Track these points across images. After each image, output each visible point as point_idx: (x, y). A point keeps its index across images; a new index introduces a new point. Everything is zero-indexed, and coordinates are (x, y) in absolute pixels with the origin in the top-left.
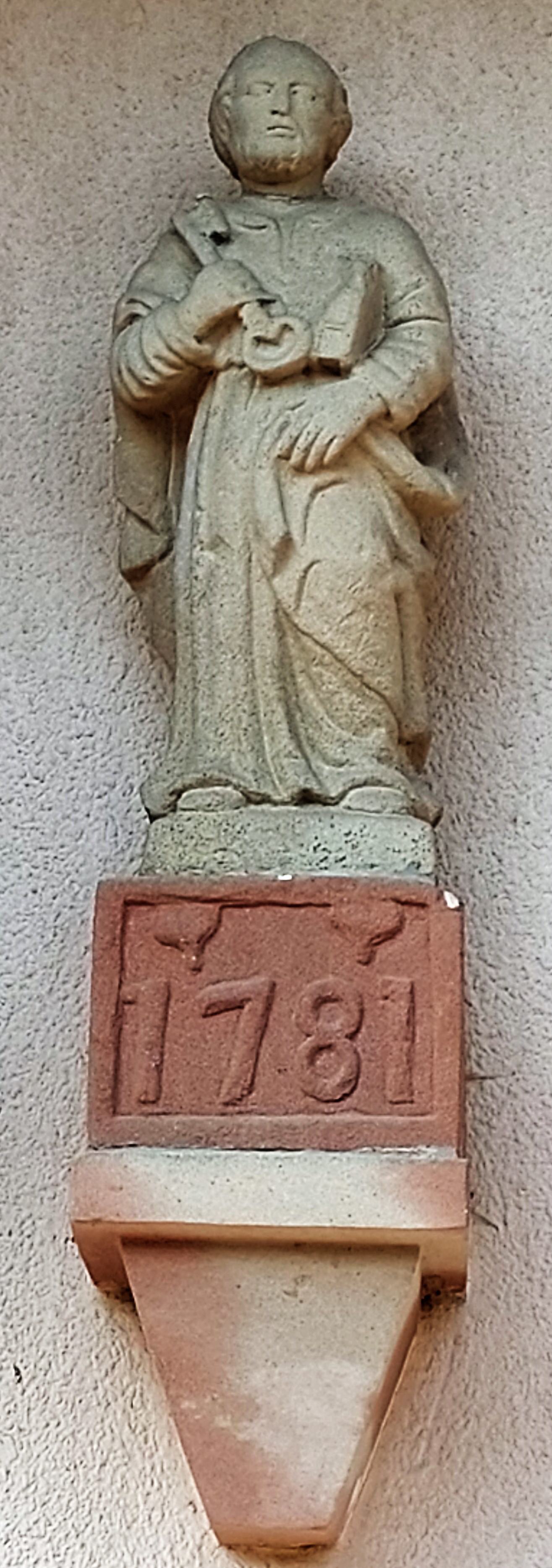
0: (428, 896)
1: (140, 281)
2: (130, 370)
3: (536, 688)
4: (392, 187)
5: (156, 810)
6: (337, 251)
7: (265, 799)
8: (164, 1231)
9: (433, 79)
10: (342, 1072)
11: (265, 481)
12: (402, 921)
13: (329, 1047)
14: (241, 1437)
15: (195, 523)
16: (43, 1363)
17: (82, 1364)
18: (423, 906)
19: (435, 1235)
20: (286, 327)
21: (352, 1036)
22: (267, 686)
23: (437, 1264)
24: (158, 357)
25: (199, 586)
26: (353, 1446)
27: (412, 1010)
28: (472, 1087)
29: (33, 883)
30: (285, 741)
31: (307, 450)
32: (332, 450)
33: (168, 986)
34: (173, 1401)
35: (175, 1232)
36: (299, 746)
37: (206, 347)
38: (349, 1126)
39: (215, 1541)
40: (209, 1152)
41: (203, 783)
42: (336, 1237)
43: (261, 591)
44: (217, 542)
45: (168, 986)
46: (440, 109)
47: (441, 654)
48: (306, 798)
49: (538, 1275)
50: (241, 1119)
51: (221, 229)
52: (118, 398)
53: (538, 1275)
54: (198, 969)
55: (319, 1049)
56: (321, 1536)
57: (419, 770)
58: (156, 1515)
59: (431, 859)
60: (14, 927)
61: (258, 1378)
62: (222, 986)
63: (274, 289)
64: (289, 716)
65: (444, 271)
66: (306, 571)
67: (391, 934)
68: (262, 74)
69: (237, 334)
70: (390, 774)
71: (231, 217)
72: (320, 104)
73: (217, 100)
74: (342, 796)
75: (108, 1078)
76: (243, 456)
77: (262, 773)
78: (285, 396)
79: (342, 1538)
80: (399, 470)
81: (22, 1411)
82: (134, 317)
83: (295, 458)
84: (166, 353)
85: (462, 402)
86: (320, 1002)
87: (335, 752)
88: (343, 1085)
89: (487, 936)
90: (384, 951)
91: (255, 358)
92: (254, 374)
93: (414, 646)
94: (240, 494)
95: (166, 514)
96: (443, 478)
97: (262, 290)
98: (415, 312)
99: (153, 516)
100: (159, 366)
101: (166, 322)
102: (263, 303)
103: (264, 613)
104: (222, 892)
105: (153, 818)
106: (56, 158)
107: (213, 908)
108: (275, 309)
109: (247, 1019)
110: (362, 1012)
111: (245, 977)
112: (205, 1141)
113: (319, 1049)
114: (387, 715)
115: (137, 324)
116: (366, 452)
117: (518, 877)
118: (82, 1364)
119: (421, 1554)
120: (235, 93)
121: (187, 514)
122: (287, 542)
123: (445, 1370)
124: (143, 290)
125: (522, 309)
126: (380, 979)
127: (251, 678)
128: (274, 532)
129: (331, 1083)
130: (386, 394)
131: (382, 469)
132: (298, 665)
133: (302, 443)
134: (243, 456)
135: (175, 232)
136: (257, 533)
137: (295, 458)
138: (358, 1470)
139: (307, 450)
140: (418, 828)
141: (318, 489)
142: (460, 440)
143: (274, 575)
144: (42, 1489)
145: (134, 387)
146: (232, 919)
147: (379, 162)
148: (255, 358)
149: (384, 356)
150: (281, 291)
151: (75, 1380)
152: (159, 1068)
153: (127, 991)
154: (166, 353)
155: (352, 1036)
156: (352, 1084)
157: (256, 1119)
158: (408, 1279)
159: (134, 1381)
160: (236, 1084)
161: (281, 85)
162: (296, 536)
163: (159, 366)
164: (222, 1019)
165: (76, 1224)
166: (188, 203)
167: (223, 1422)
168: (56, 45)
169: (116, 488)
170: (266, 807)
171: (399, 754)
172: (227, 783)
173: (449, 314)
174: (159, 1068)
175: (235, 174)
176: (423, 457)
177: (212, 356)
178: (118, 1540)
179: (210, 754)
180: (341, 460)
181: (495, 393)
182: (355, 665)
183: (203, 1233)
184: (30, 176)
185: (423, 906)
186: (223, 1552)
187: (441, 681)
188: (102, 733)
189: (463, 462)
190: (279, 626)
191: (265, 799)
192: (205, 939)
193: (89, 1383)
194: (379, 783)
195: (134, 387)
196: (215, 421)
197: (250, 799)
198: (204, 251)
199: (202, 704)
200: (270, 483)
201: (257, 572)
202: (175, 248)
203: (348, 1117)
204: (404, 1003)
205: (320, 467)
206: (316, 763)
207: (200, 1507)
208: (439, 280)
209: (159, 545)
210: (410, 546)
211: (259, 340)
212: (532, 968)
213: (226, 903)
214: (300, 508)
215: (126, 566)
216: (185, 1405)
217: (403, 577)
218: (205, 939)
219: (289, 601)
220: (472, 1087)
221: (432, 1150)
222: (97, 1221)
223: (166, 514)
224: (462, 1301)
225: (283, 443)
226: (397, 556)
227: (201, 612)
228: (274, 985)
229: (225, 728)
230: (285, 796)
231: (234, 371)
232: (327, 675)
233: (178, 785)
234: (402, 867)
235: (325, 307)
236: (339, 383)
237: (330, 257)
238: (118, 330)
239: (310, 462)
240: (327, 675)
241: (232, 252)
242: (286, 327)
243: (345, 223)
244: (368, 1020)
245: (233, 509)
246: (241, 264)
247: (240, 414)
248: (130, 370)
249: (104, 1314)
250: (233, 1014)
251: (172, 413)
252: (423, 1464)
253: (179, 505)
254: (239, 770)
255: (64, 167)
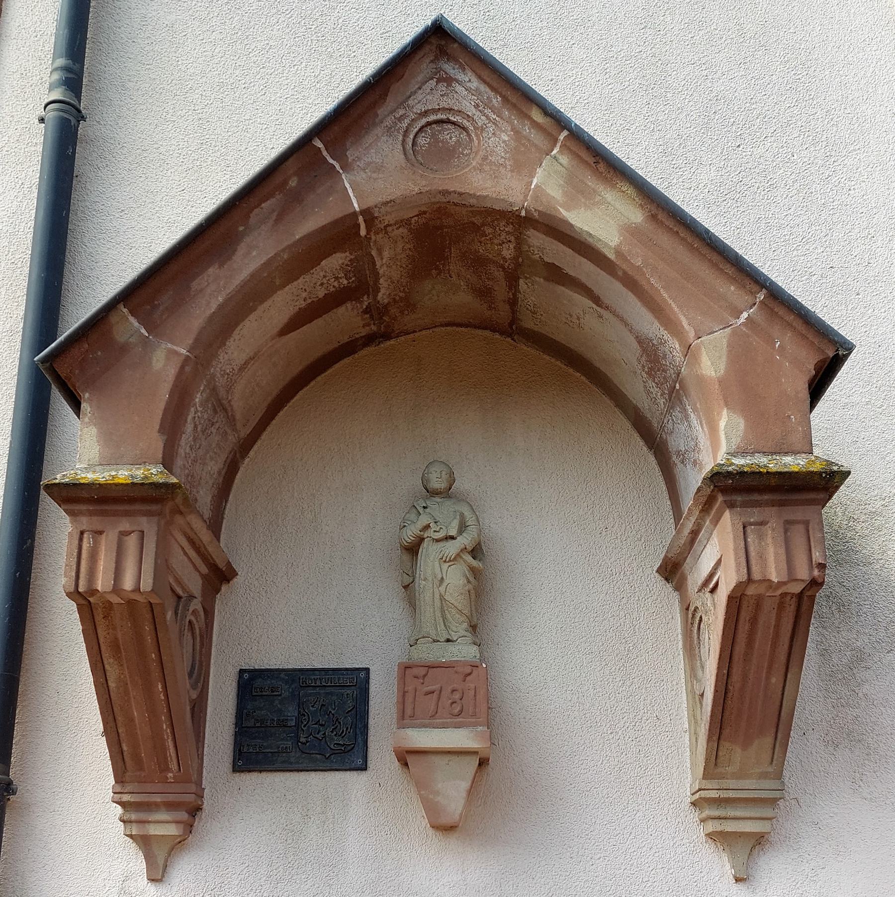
0: (478, 664)
1: (405, 518)
2: (404, 539)
3: (502, 612)
4: (465, 494)
5: (412, 644)
6: (453, 510)
7: (438, 641)
8: (416, 749)
9: (474, 468)
10: (459, 709)
11: (437, 564)
12: (472, 671)
13: (455, 702)
14: (436, 800)
15: (420, 574)
16: (386, 782)
17: (396, 782)
18: (477, 667)
19: (482, 749)
20: (441, 528)
21: (461, 699)
22: (438, 614)
23: (482, 756)
24: (411, 536)
25: (421, 590)
26: (463, 802)
27: (475, 693)
28: (490, 711)
29: (382, 662)
30: (443, 627)
31: (447, 557)
32: (453, 557)
33: (416, 688)
34: (419, 791)
35: (418, 749)
36: (446, 628)
37: (422, 533)
38: (461, 722)
39: (429, 826)
40: (427, 729)
41: (423, 637)
42: (458, 750)
43: (436, 590)
44: (425, 579)
45: (416, 688)
46: (476, 476)
47: (479, 604)
48: (448, 640)
49: (507, 757)
50: (434, 721)
51: (425, 505)
52: (401, 545)
53: (507, 757)
54: (423, 684)
55: (453, 703)
56: (456, 824)
57: (475, 633)
58: (414, 820)
59: (479, 655)
60: (377, 673)
61: (440, 786)
62: (429, 688)
63: (438, 519)
64: (444, 620)
65: (477, 513)
66: (446, 588)
67: (470, 674)
68: (434, 469)
69: (429, 530)
70: (469, 634)
71: (427, 503)
72: (448, 475)
73: (423, 475)
74: (457, 640)
75: (402, 711)
76: (431, 559)
77: (437, 635)
78: (441, 544)
79: (460, 825)
80: (469, 561)
81: (381, 794)
82: (405, 526)
83: (444, 559)
84: (413, 535)
85: (483, 544)
86: (453, 691)
87: (455, 629)
88: (460, 711)
89: (492, 673)
90: (468, 678)
91: (433, 535)
92: (433, 539)
93: (473, 603)
94: (431, 568)
95: (413, 572)
96: (479, 563)
97: (435, 519)
98: (472, 524)
99: (410, 573)
100: (411, 538)
101: (412, 527)
102: (435, 522)
103: (437, 596)
104: (429, 664)
105: (411, 646)
106: (385, 489)
107: (427, 668)
108: (438, 524)
109: (435, 695)
110: (463, 693)
111: (435, 685)
112: (425, 726)
113: (453, 703)
114: (467, 620)
115: (405, 528)
116: (461, 557)
117: (499, 658)
118: (396, 782)
119: (480, 828)
120: (428, 473)
121: (418, 573)
122: (442, 578)
123: (485, 781)
124: (407, 520)
125: (497, 522)
126: (467, 685)
127: (434, 612)
128: (440, 576)
129: (456, 711)
130: (466, 544)
131: (465, 561)
132: (445, 608)
133: (445, 555)
134: (431, 559)
135: (414, 506)
136: (435, 577)
137: (444, 559)
138: (465, 807)
139: (447, 557)
140: (476, 647)
141: (450, 566)
142: (483, 553)
143: (440, 586)
144: (386, 813)
145: (405, 542)
146: (431, 671)
147: (462, 488)
148: (433, 535)
149: (464, 534)
150: (440, 519)
151: (394, 786)
152: (414, 708)
153: (406, 689)
154: (413, 535)
155: (461, 699)
156: (461, 711)
157: (438, 720)
158: (476, 760)
159: (408, 786)
160: (432, 712)
161: (439, 472)
162: (444, 577)
163: (411, 538)
164: (429, 695)
165: (394, 748)
166: (417, 498)
167: (431, 796)
168: (384, 463)
169: (400, 566)
170: (438, 643)
171: (470, 629)
172: (429, 637)
173: (479, 523)
174: (414, 708)
175: (428, 492)
176: (474, 558)
177: (423, 535)
178: (405, 826)
179: (425, 630)
180: (455, 559)
181: (490, 542)
182: (459, 608)
183: (425, 750)
184: (379, 493)
185: (477, 667)
186: (431, 829)
187: (479, 611)
188: (398, 625)
189: (483, 558)
190: (441, 599)
191: (438, 641)
192: (425, 676)
193: (397, 787)
194: (466, 636)
195: (405, 542)
196: (424, 550)
197: (434, 641)
198: (421, 510)
199: (422, 618)
200: (438, 565)
201: (435, 586)
202: (414, 510)
203: (461, 720)
204: (473, 691)
205: (450, 561)
206: (450, 632)
207: (426, 817)
208: (477, 515)
209: (411, 580)
210: (472, 579)
211: (435, 531)
212: (504, 681)
213: (429, 667)
214: (445, 571)
215: (404, 585)
216: (422, 792)
217: (470, 586)
218: (425, 676)
219: (443, 593)
220: (490, 711)
221: (481, 728)
222: (400, 747)
223: (413, 572)
224: (488, 764)
225: (441, 555)
226: (469, 582)
227: (422, 596)
228: (441, 687)
229: (428, 624)
230: (443, 640)
231: (429, 538)
232: (453, 611)
233: (417, 638)
234: (472, 657)
235: (450, 523)
236: (454, 541)
237: (451, 511)
238: (401, 529)
239: (447, 560)
240: (453, 611)
241: (427, 510)
242: (441, 528)
243: (454, 503)
244: (464, 696)
245: (429, 571)
246: (430, 514)
247: (430, 549)
248: (404, 539)
249: (401, 769)
250: (432, 694)
251: (414, 548)
252: (480, 805)
253: (416, 570)
254: (432, 634)
255: (387, 491)
